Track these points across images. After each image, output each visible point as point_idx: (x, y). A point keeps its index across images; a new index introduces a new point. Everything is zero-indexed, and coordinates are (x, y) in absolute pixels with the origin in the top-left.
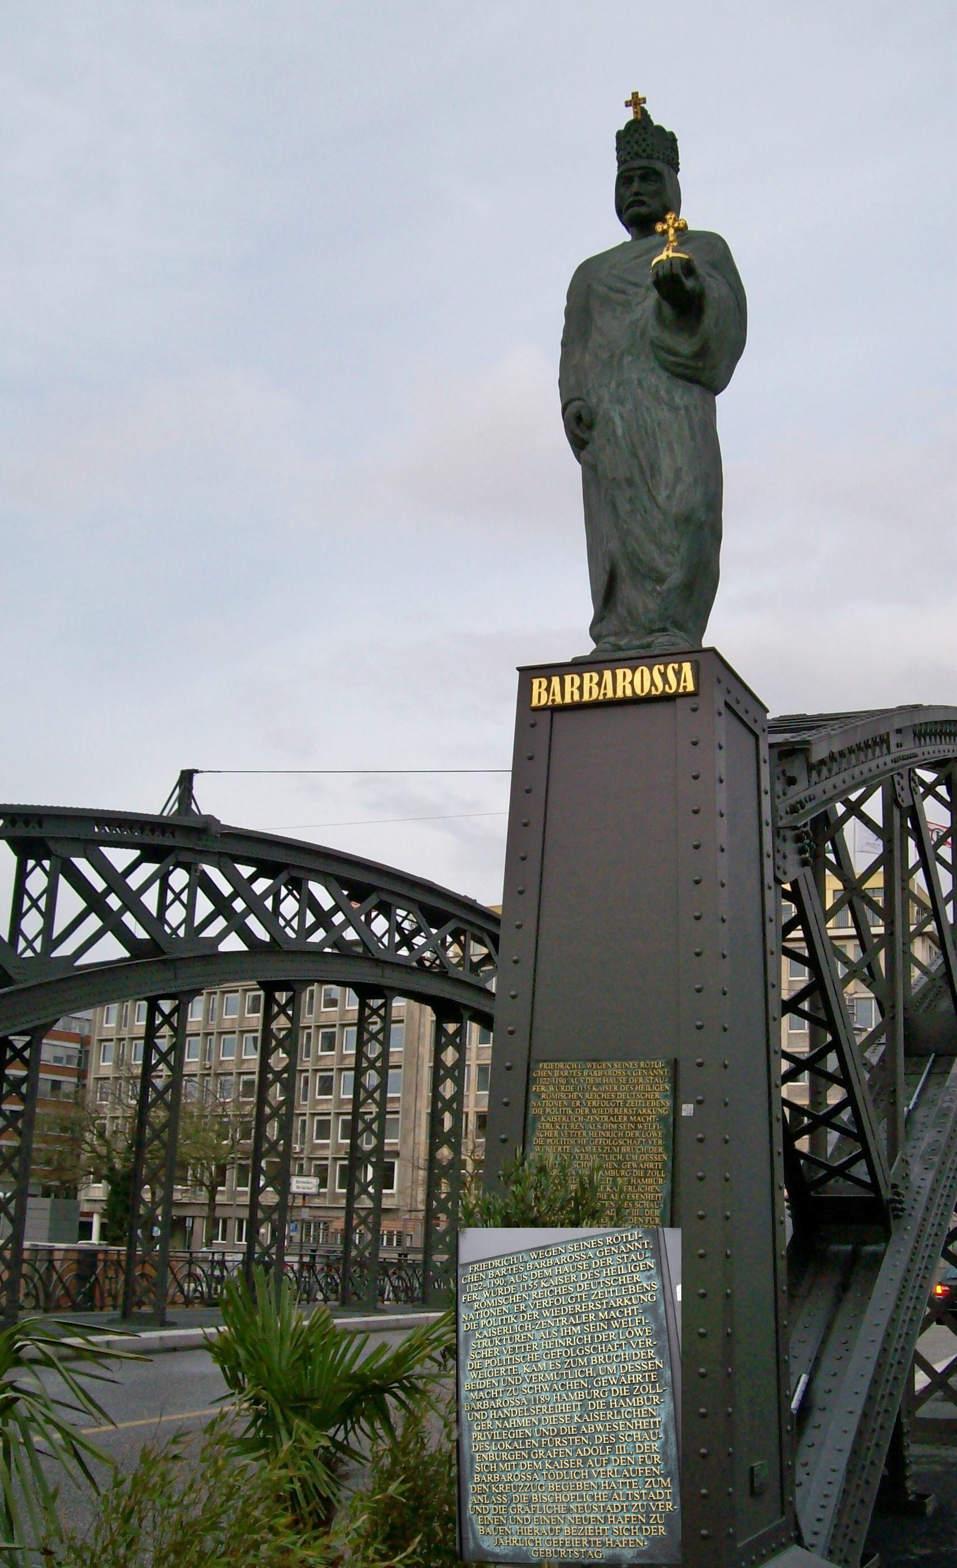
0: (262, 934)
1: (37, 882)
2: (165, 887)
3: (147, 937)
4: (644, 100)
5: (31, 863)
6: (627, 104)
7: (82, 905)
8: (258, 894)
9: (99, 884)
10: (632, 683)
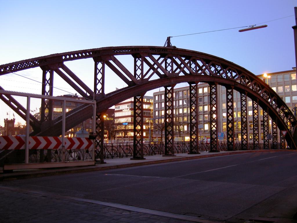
5: (137, 59)
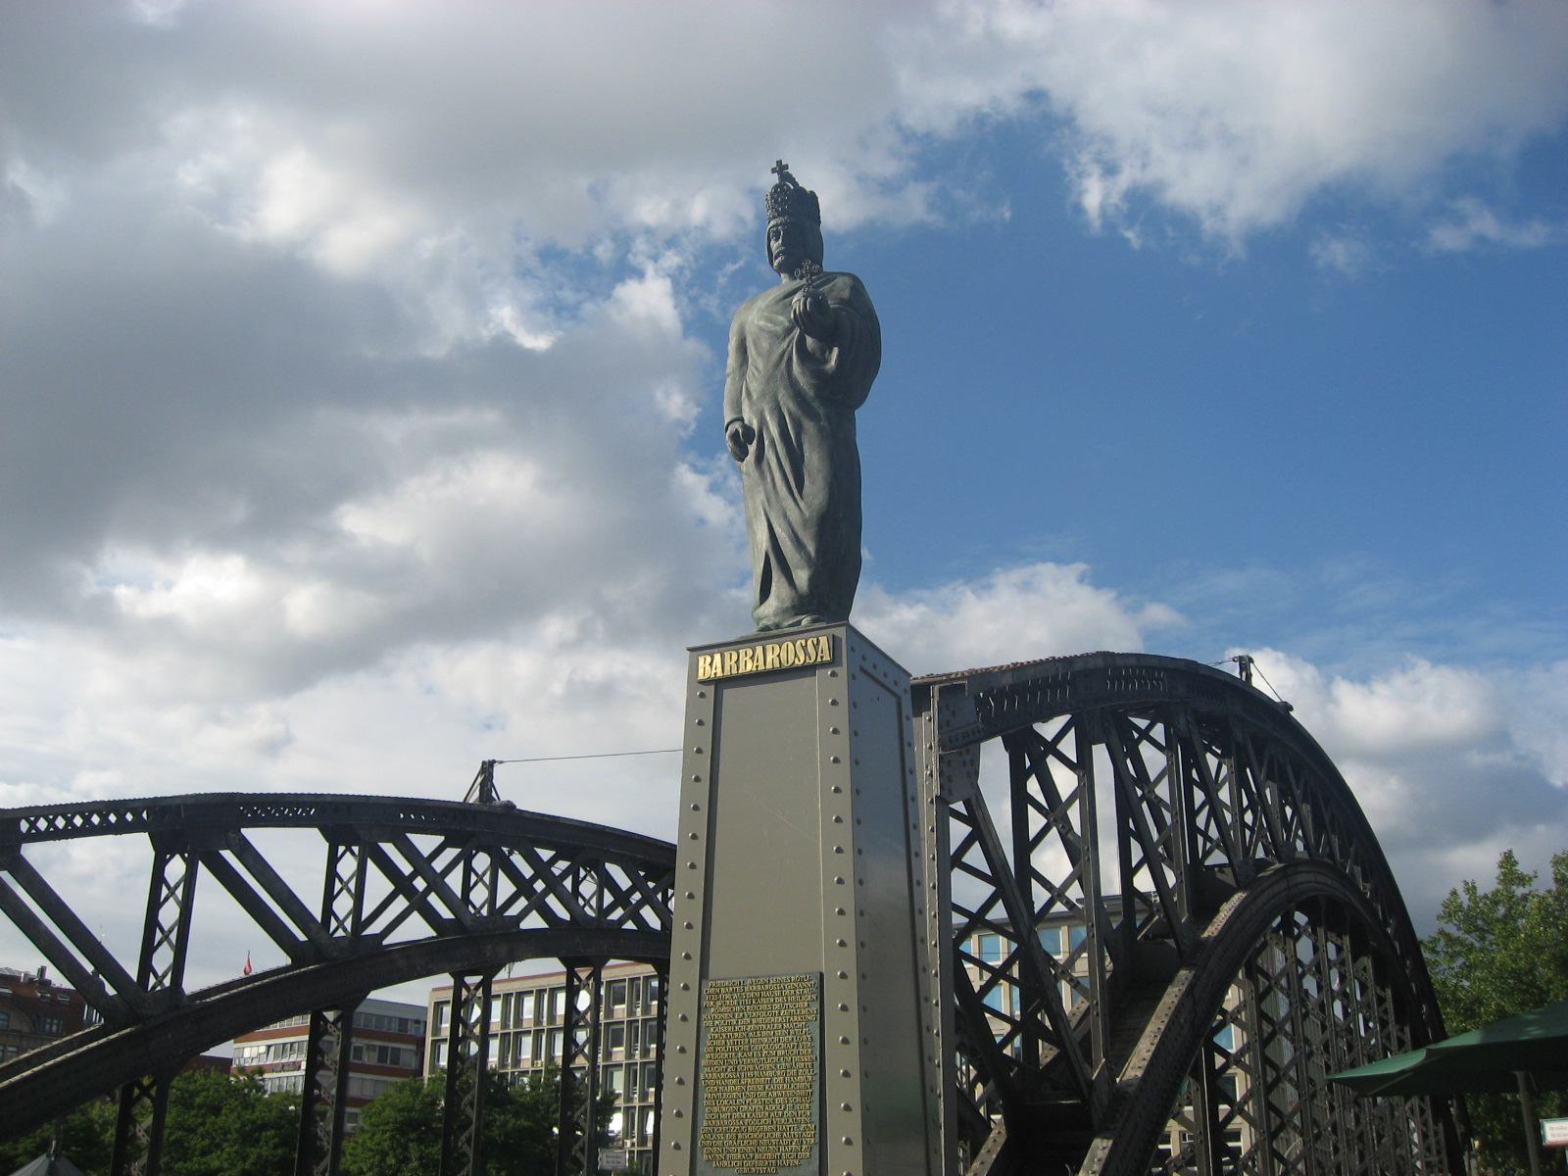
0: (563, 914)
1: (347, 866)
2: (468, 870)
3: (453, 917)
4: (787, 167)
5: (341, 849)
6: (773, 171)
7: (390, 887)
8: (624, 890)
9: (406, 868)
10: (779, 656)
